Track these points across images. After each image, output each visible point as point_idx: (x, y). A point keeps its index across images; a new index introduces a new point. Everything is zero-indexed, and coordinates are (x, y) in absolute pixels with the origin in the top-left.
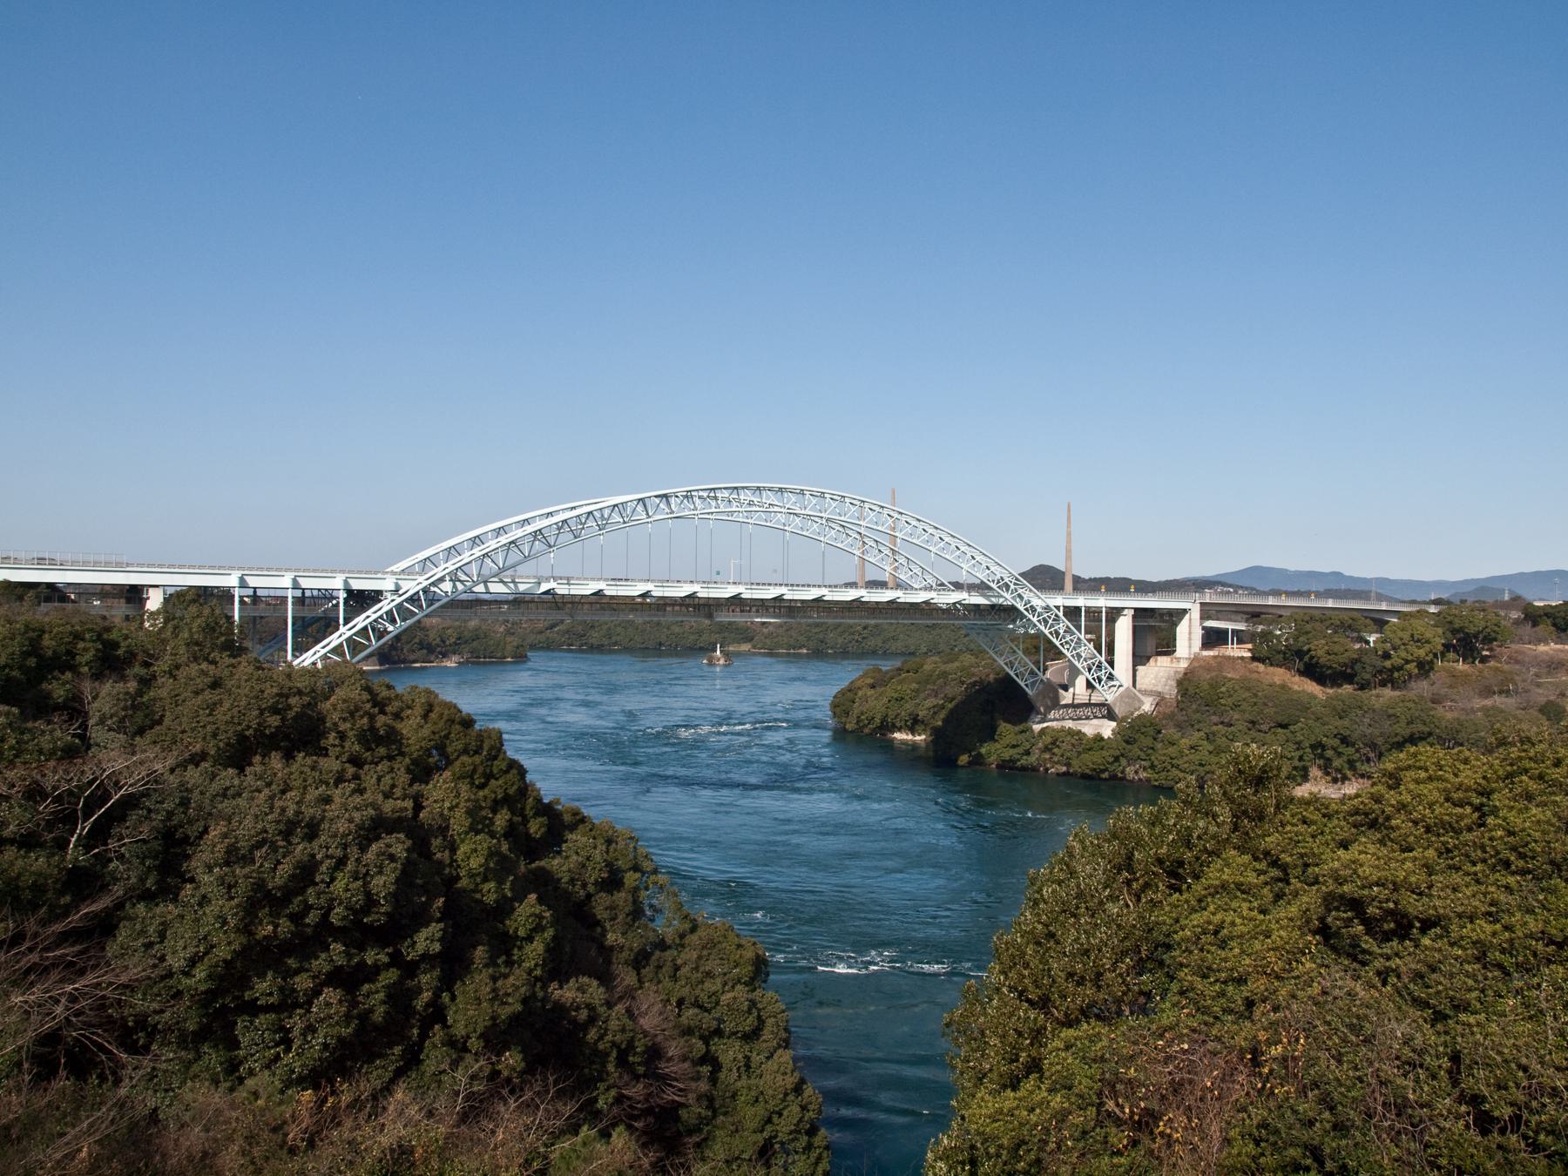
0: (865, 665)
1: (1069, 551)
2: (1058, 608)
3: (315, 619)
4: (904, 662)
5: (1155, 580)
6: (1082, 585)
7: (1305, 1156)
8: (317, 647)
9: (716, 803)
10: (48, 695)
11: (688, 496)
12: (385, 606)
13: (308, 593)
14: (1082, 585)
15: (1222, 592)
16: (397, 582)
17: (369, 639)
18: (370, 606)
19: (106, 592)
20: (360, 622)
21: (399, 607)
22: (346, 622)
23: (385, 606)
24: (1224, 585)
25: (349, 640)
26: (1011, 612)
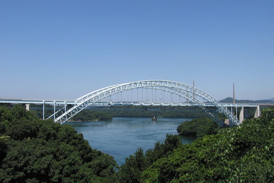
0: (184, 120)
1: (234, 94)
3: (60, 110)
4: (193, 120)
6: (237, 102)
7: (16, 114)
8: (71, 109)
9: (111, 140)
10: (254, 147)
11: (141, 83)
12: (75, 107)
13: (59, 105)
14: (237, 102)
16: (79, 102)
17: (71, 114)
18: (72, 107)
19: (20, 105)
20: (69, 111)
21: (77, 108)
22: (66, 111)
25: (61, 118)
26: (215, 108)
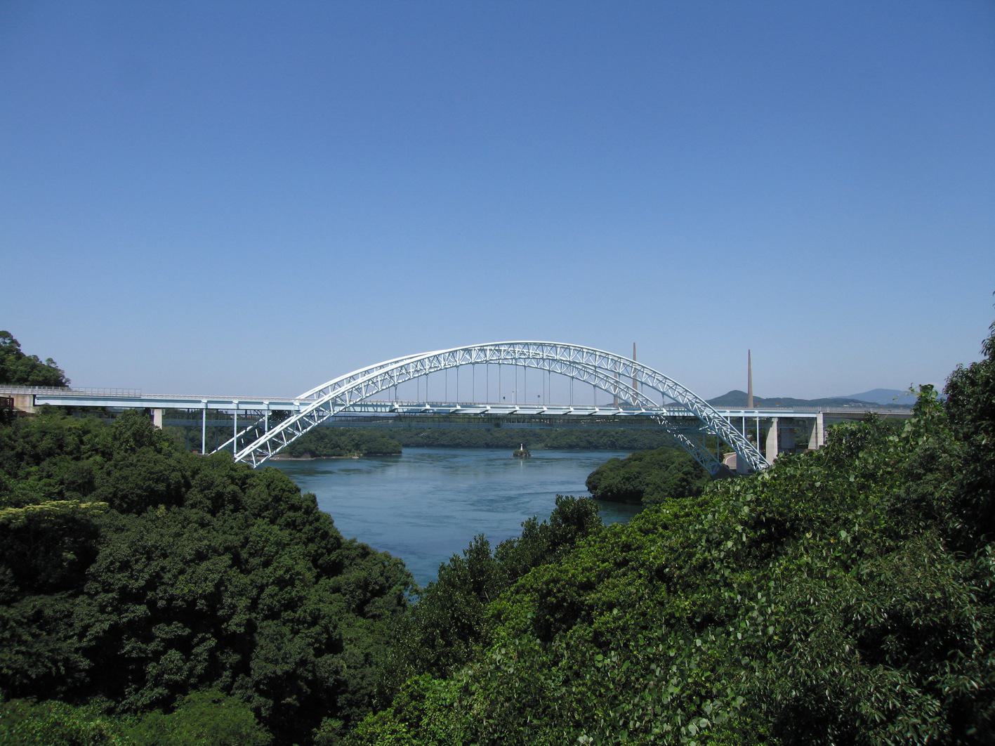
2: (726, 418)
3: (252, 426)
5: (764, 397)
6: (759, 403)
10: (808, 532)
11: (482, 350)
12: (293, 419)
13: (249, 413)
14: (759, 403)
15: (855, 407)
16: (305, 403)
17: (282, 439)
18: (284, 419)
19: (135, 411)
20: (278, 429)
21: (301, 420)
22: (269, 429)
23: (293, 419)
24: (857, 402)
26: (697, 421)
